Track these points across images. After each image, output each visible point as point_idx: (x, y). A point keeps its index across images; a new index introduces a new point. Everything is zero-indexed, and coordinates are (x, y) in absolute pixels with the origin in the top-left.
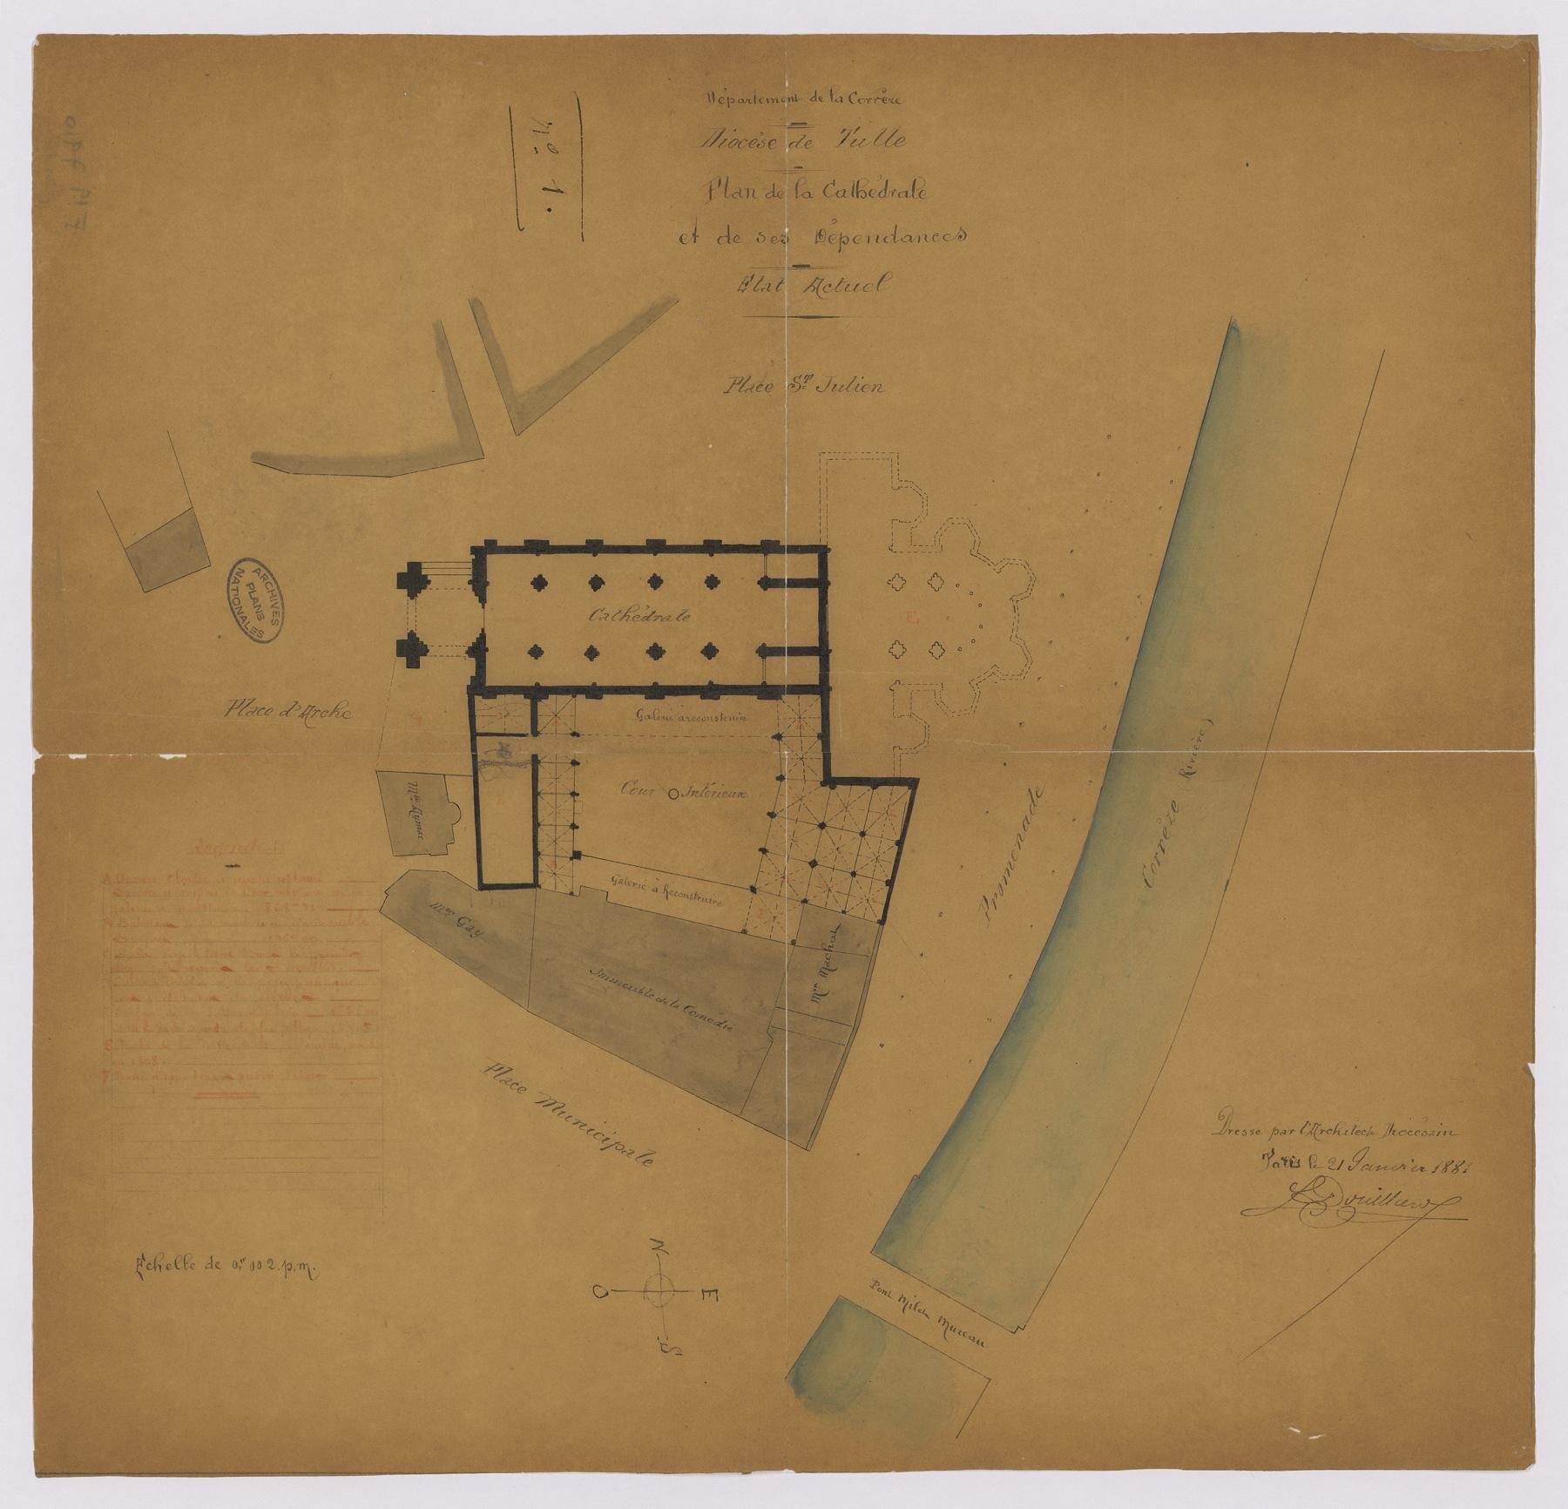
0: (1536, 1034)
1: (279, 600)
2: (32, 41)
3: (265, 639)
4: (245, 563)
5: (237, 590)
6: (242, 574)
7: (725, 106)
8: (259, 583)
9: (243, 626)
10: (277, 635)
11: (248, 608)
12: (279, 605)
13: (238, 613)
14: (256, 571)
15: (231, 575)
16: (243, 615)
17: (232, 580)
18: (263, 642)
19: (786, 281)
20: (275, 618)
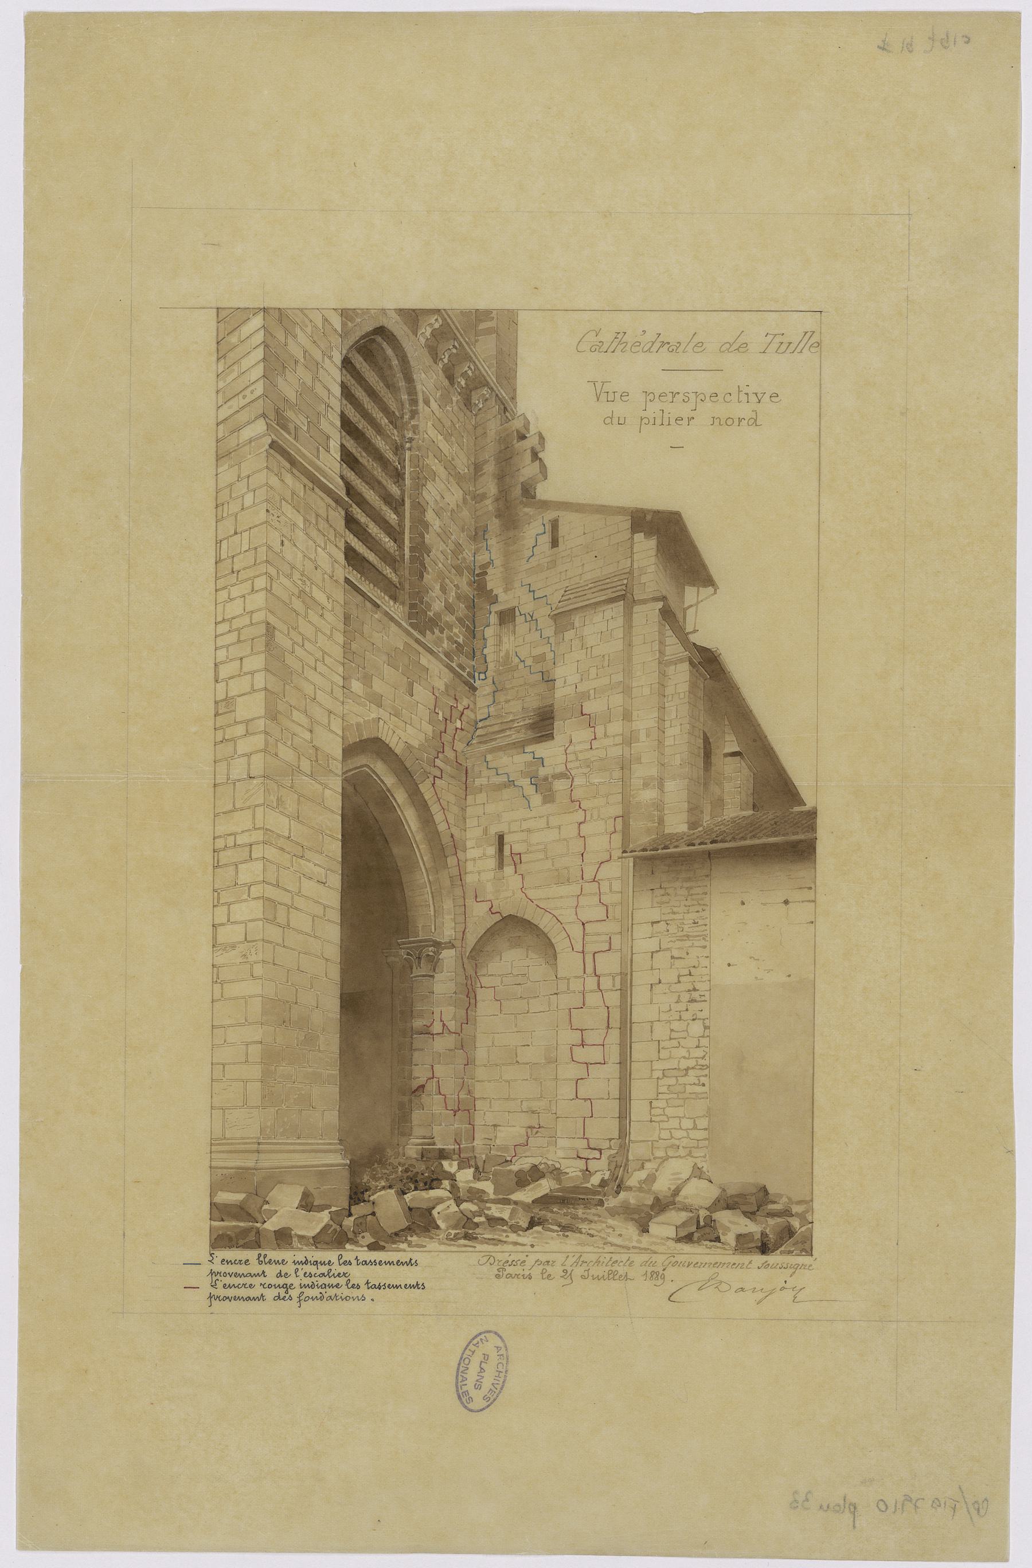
0: (428, 308)
1: (501, 1383)
2: (1010, 1560)
3: (470, 1406)
4: (492, 1334)
5: (473, 1352)
6: (481, 1380)
7: (616, 415)
8: (494, 1356)
9: (459, 1384)
10: (481, 1410)
11: (472, 1374)
12: (499, 1387)
13: (462, 1372)
14: (497, 1347)
15: (476, 1337)
16: (465, 1375)
17: (475, 1342)
18: (466, 1407)
19: (295, 442)
20: (488, 1395)
